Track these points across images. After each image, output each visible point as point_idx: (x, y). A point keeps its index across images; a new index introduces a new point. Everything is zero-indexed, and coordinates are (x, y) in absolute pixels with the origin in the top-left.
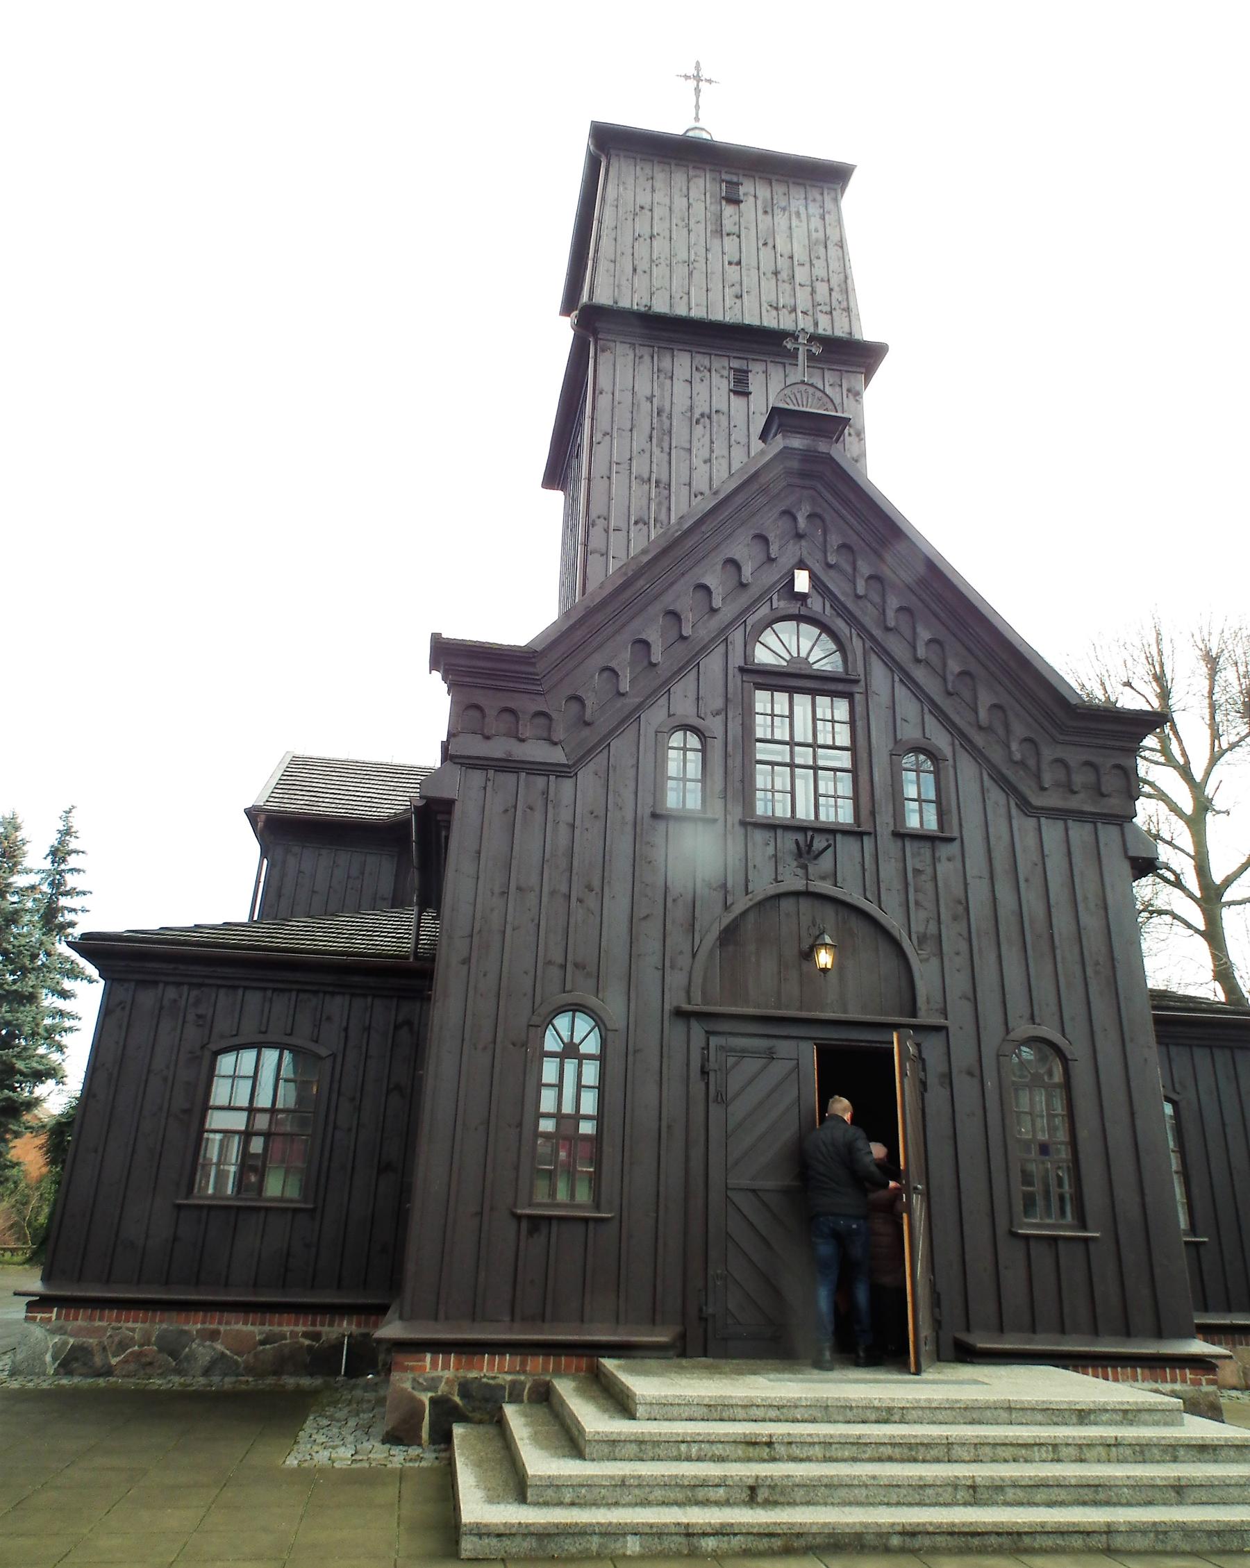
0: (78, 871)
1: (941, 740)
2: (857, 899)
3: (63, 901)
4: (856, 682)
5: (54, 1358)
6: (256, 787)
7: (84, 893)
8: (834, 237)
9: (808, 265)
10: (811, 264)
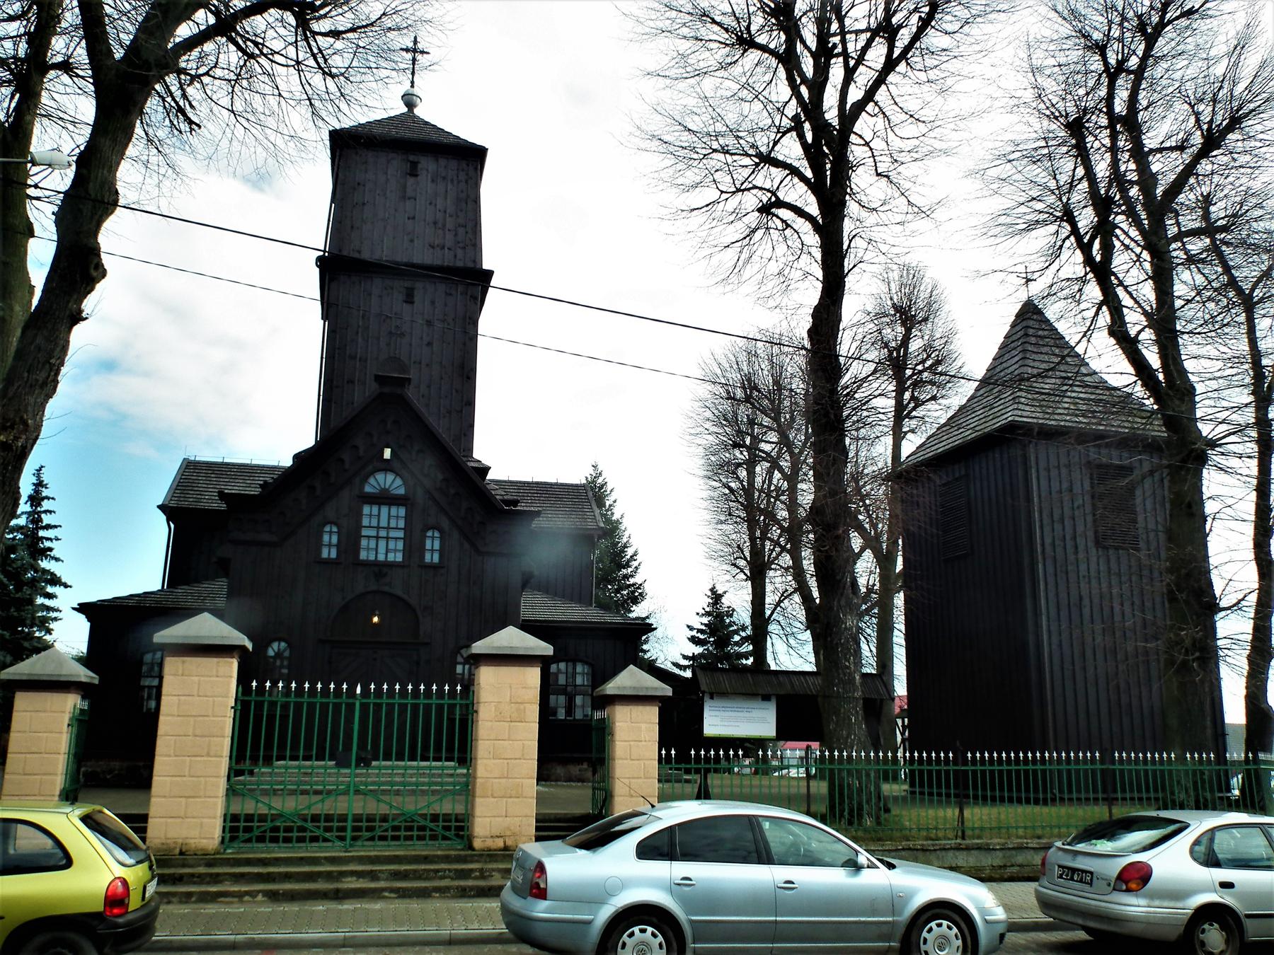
0: (50, 512)
1: (445, 523)
2: (399, 592)
3: (42, 533)
6: (161, 493)
7: (56, 527)
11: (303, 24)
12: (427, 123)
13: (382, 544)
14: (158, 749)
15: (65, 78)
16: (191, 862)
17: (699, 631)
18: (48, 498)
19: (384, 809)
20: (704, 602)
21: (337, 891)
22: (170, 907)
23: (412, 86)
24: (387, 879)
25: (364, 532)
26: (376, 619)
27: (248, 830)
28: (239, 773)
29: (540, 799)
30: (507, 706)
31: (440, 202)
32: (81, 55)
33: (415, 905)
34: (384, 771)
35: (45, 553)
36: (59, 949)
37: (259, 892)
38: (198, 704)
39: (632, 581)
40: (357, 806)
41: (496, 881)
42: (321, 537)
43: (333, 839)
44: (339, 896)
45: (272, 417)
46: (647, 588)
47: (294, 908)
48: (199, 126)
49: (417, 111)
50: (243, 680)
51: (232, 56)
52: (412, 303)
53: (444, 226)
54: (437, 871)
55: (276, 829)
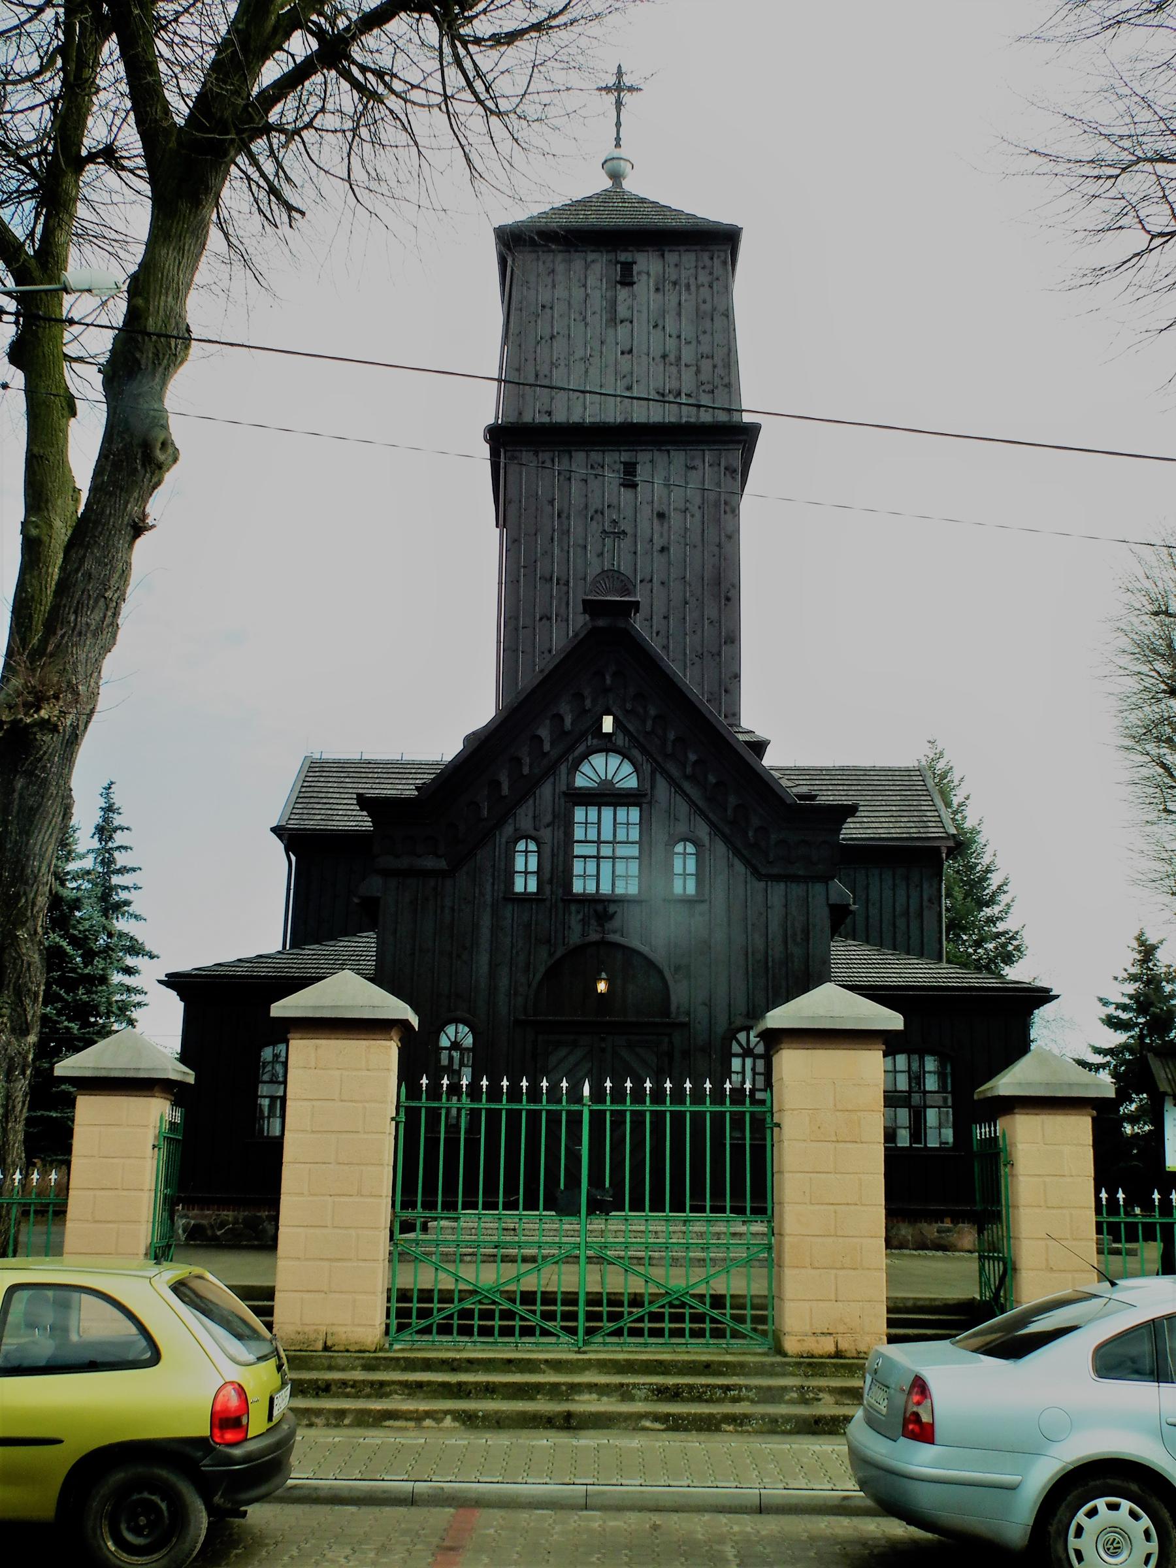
0: (126, 848)
1: (703, 831)
3: (116, 880)
4: (646, 795)
5: (184, 1232)
6: (275, 811)
7: (134, 870)
8: (721, 308)
9: (694, 343)
10: (699, 342)
11: (448, 26)
12: (643, 201)
13: (606, 866)
14: (283, 1190)
15: (110, 178)
16: (341, 1362)
17: (1119, 1006)
18: (122, 829)
19: (636, 1285)
20: (1127, 959)
21: (569, 1416)
22: (312, 1432)
23: (618, 145)
24: (646, 1399)
25: (578, 850)
26: (602, 987)
27: (424, 1314)
28: (407, 1227)
29: (892, 1279)
30: (832, 1113)
31: (670, 326)
32: (130, 140)
33: (695, 1443)
34: (626, 1229)
35: (119, 907)
36: (146, 1495)
37: (446, 1412)
38: (340, 1109)
39: (1001, 927)
40: (583, 1280)
41: (827, 1407)
42: (511, 861)
43: (557, 1331)
44: (569, 1423)
45: (427, 687)
46: (1028, 939)
47: (500, 1440)
48: (303, 213)
49: (628, 185)
50: (408, 1074)
51: (345, 97)
52: (634, 486)
53: (679, 358)
54: (728, 1388)
55: (466, 1314)
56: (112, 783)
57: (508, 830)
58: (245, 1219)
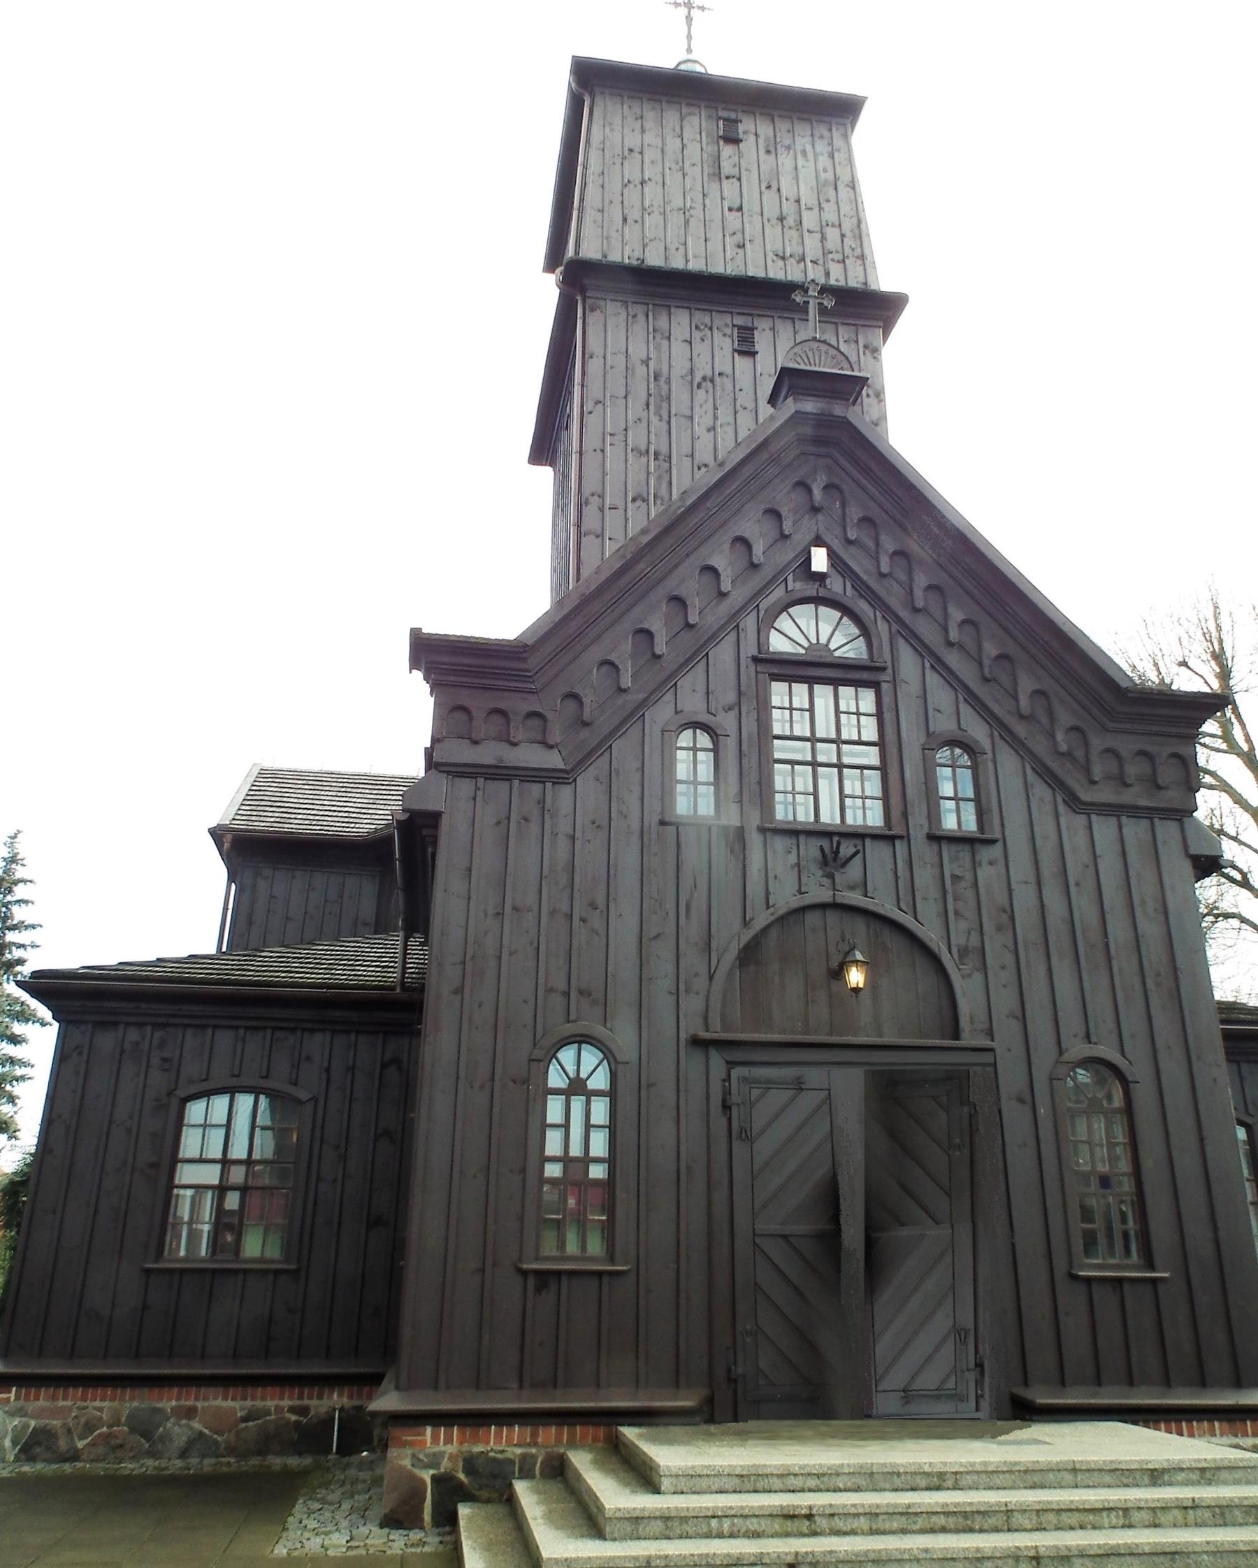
0: (26, 902)
3: (11, 937)
4: (883, 669)
5: (14, 1443)
6: (222, 805)
7: (34, 927)
8: (844, 177)
9: (816, 209)
18: (24, 881)
25: (781, 750)
42: (668, 765)
52: (753, 354)
56: (19, 832)
57: (661, 714)
58: (132, 1416)
